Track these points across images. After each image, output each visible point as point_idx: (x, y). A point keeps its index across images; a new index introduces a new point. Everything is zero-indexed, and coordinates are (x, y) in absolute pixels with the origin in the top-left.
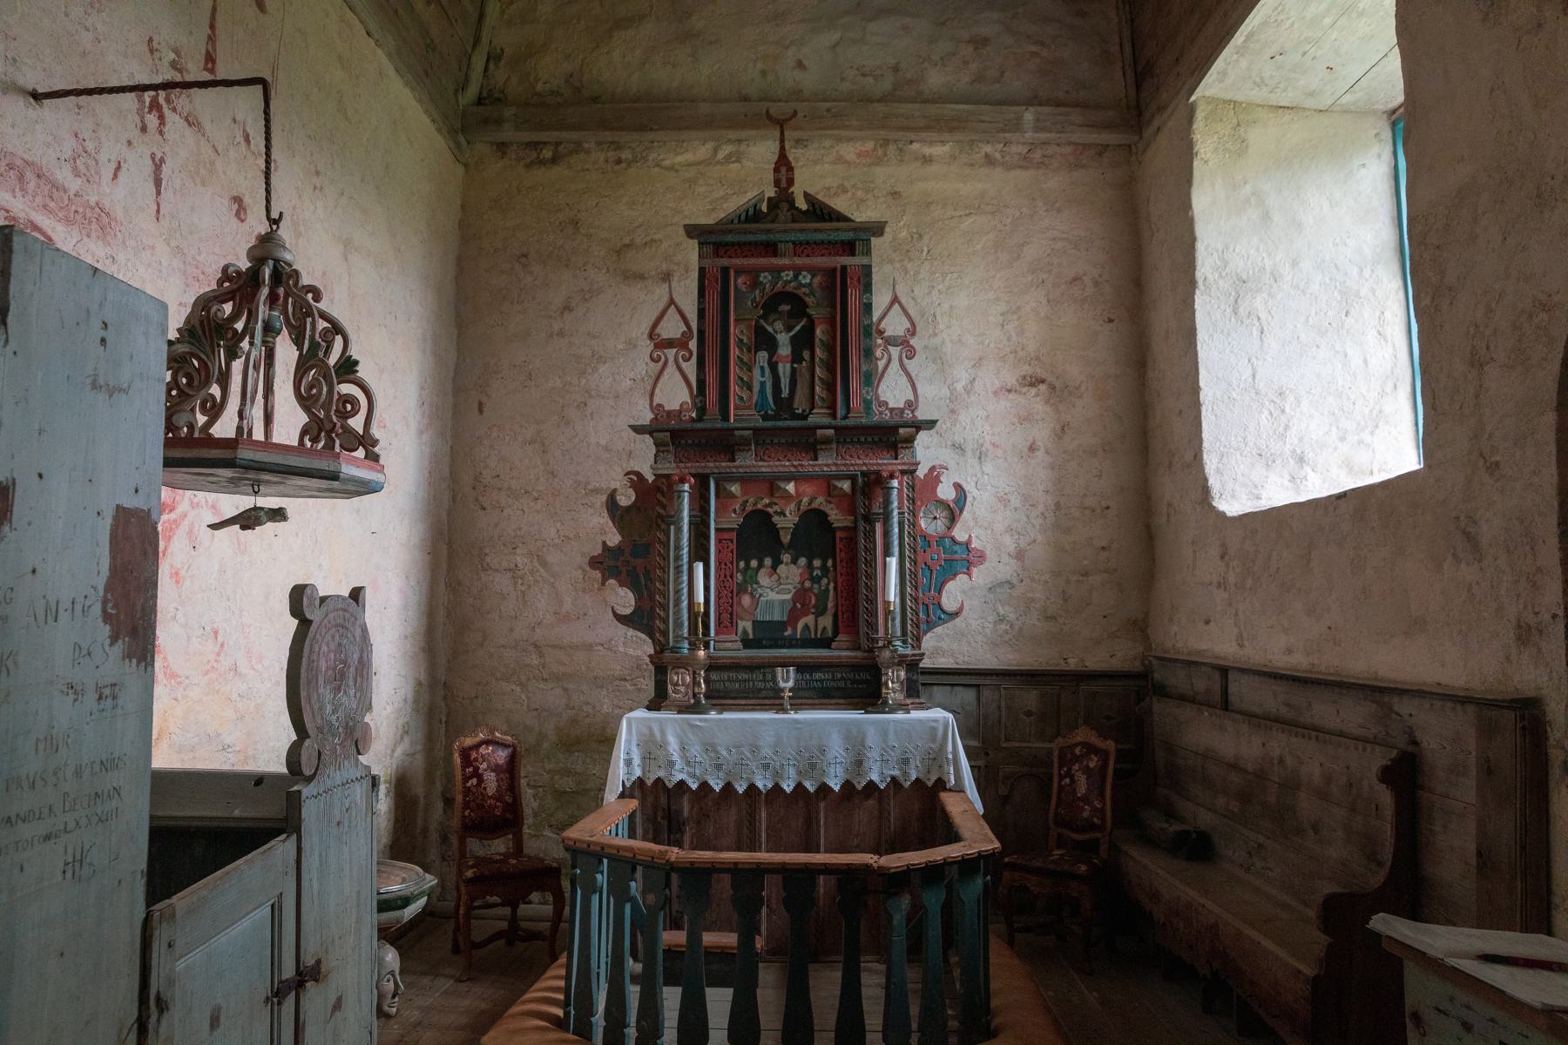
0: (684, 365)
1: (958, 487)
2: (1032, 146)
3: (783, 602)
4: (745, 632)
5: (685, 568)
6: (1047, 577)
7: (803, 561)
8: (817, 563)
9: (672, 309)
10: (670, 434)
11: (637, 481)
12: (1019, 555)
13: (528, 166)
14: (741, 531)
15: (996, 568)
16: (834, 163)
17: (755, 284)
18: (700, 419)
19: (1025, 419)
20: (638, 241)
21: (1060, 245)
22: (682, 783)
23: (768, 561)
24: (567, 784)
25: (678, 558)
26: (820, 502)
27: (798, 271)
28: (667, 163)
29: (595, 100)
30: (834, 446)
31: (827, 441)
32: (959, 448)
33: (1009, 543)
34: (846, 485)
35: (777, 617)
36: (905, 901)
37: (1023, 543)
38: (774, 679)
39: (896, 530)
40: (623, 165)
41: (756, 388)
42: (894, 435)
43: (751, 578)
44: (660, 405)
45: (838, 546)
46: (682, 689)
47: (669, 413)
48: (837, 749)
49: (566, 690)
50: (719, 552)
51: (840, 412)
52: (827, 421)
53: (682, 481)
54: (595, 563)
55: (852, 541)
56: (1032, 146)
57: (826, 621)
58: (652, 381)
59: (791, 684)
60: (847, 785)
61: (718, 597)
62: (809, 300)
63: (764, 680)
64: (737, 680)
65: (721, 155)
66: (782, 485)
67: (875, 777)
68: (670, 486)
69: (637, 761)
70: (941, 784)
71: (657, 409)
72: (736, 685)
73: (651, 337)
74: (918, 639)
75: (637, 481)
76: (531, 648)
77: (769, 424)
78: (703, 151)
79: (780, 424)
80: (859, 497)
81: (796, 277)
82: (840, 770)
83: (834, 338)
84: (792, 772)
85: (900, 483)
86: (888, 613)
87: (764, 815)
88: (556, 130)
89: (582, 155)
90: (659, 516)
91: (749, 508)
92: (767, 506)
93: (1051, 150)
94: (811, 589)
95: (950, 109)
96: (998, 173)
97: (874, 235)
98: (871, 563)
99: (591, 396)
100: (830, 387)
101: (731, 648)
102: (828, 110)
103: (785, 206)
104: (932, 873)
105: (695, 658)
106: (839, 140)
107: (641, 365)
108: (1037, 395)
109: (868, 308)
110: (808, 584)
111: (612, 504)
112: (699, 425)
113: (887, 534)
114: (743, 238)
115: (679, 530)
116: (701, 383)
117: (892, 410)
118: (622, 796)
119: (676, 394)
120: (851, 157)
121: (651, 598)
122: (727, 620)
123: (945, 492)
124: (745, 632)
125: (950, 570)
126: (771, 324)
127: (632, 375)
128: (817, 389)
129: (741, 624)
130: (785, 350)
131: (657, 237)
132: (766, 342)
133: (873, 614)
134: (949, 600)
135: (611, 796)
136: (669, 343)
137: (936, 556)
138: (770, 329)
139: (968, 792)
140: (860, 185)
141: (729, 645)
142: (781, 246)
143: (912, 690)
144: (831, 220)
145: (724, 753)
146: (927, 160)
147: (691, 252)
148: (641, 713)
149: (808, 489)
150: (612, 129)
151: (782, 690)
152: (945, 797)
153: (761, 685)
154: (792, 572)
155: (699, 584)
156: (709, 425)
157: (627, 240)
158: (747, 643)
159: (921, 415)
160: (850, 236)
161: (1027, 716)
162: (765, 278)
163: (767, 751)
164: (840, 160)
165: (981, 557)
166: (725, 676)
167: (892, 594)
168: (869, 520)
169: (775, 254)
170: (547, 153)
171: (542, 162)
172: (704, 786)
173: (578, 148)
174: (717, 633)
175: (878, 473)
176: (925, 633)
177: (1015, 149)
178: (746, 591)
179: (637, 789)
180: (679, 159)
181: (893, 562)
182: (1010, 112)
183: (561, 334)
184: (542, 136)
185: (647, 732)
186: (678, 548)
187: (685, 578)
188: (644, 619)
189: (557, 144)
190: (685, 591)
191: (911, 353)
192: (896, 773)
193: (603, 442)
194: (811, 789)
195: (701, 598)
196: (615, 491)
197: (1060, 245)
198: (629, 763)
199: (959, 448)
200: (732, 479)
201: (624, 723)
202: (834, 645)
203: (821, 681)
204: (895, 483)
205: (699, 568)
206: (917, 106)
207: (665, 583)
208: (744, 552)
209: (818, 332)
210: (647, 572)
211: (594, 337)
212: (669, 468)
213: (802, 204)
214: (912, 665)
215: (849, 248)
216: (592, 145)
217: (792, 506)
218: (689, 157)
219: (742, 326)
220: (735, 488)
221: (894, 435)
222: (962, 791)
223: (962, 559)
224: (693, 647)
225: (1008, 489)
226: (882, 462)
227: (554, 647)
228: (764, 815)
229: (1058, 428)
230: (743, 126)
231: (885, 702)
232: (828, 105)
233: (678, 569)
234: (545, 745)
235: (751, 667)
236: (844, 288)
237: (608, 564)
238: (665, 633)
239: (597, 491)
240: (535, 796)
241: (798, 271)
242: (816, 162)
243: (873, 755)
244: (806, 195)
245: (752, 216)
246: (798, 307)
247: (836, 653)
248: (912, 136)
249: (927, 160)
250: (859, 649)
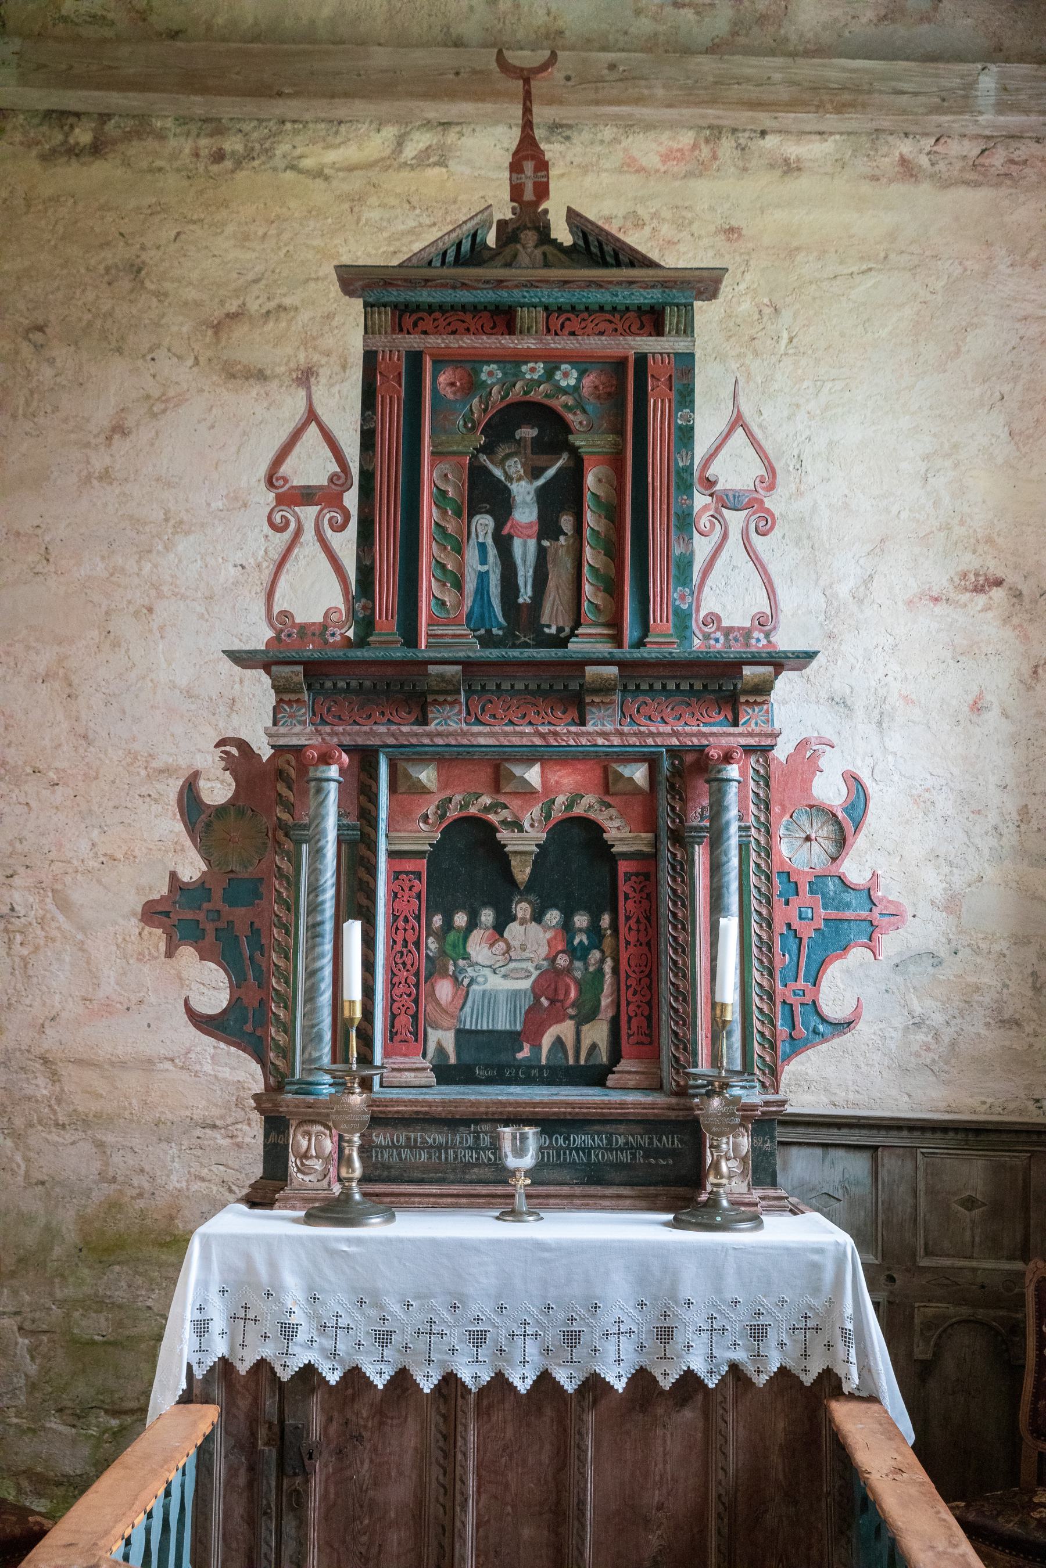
0: (336, 540)
1: (853, 780)
2: (989, 142)
3: (515, 994)
4: (441, 1050)
5: (328, 927)
6: (1002, 946)
7: (553, 916)
8: (581, 920)
9: (313, 427)
10: (305, 670)
11: (238, 756)
12: (952, 904)
13: (47, 158)
14: (436, 855)
15: (919, 930)
16: (620, 171)
17: (472, 386)
18: (361, 641)
19: (965, 653)
20: (253, 306)
21: (1033, 330)
22: (309, 1369)
23: (487, 916)
24: (95, 1326)
25: (314, 908)
26: (588, 805)
27: (553, 362)
28: (308, 163)
29: (174, 35)
30: (617, 697)
31: (604, 689)
32: (841, 704)
33: (933, 883)
34: (639, 774)
35: (502, 1024)
37: (959, 881)
38: (496, 1147)
39: (735, 862)
40: (228, 164)
41: (470, 585)
42: (729, 681)
44: (285, 614)
45: (623, 891)
46: (318, 1165)
47: (303, 628)
48: (619, 1300)
49: (100, 1145)
50: (394, 896)
51: (630, 632)
52: (604, 649)
53: (326, 759)
54: (152, 913)
56: (989, 142)
57: (597, 1033)
58: (272, 568)
59: (528, 1161)
60: (642, 1378)
61: (391, 984)
62: (574, 419)
63: (476, 1148)
64: (425, 1146)
65: (410, 151)
66: (517, 770)
67: (698, 1364)
68: (303, 769)
69: (218, 1323)
70: (830, 1383)
72: (424, 1157)
73: (270, 482)
74: (774, 1072)
75: (238, 756)
76: (38, 1065)
77: (494, 654)
78: (376, 143)
79: (515, 653)
80: (663, 796)
81: (549, 374)
82: (627, 1346)
83: (620, 491)
84: (532, 1349)
85: (743, 772)
86: (719, 1027)
87: (472, 1438)
88: (98, 87)
89: (151, 144)
90: (281, 825)
91: (453, 814)
92: (487, 809)
93: (1025, 150)
94: (568, 970)
95: (837, 70)
96: (924, 193)
97: (701, 295)
98: (685, 924)
99: (160, 596)
100: (612, 587)
101: (408, 1079)
102: (612, 67)
103: (530, 237)
105: (347, 1110)
106: (630, 126)
107: (260, 543)
108: (987, 609)
109: (686, 435)
110: (562, 961)
111: (190, 801)
112: (360, 654)
113: (716, 868)
114: (450, 296)
115: (317, 853)
116: (365, 573)
117: (728, 631)
118: (186, 1398)
119: (316, 594)
120: (652, 160)
121: (262, 983)
122: (407, 1029)
123: (829, 790)
124: (441, 1050)
125: (835, 939)
126: (501, 463)
127: (239, 557)
128: (587, 589)
129: (434, 1036)
130: (525, 514)
131: (287, 301)
132: (488, 496)
133: (688, 1021)
135: (164, 1396)
136: (306, 496)
137: (805, 913)
138: (498, 473)
139: (887, 1401)
140: (666, 214)
141: (409, 1077)
142: (522, 313)
143: (762, 1171)
144: (618, 264)
145: (396, 1308)
146: (790, 168)
147: (348, 329)
148: (235, 1221)
149: (567, 779)
150: (205, 91)
151: (513, 1173)
152: (842, 1412)
153: (470, 1156)
154: (533, 938)
155: (347, 964)
156: (379, 654)
157: (232, 307)
158: (446, 1074)
159: (785, 641)
160: (654, 296)
162: (490, 374)
163: (481, 1306)
164: (631, 166)
165: (896, 915)
166: (401, 1136)
167: (729, 993)
168: (681, 838)
169: (510, 329)
170: (83, 136)
171: (73, 152)
172: (354, 1376)
173: (141, 127)
174: (386, 1055)
175: (701, 751)
176: (788, 1059)
177: (955, 148)
178: (444, 974)
179: (217, 1384)
180: (331, 156)
181: (730, 926)
182: (951, 75)
183: (106, 476)
184: (71, 99)
185: (241, 1264)
186: (315, 889)
187: (328, 947)
188: (242, 1025)
189: (104, 117)
190: (328, 972)
192: (740, 1355)
193: (183, 682)
194: (570, 1387)
195: (354, 991)
196: (196, 775)
197: (1033, 330)
198: (202, 1328)
199: (841, 704)
200: (422, 756)
201: (195, 1247)
202: (611, 1080)
203: (587, 1150)
204: (733, 771)
205: (354, 930)
206: (779, 61)
207: (289, 954)
209: (590, 480)
210: (255, 932)
211: (169, 485)
212: (301, 733)
213: (562, 234)
215: (653, 319)
216: (169, 123)
217: (536, 811)
219: (445, 467)
220: (427, 776)
221: (729, 681)
222: (873, 1399)
223: (851, 918)
225: (930, 782)
226: (712, 732)
227: (80, 1062)
228: (472, 1438)
229: (1026, 670)
230: (451, 95)
231: (713, 1203)
232: (611, 56)
233: (314, 928)
234: (57, 1251)
235: (452, 1122)
236: (641, 399)
237: (180, 917)
238: (286, 1052)
239: (167, 771)
240: (33, 1351)
241: (553, 362)
242: (585, 169)
243: (691, 1322)
244: (572, 215)
245: (468, 253)
246: (553, 431)
247: (616, 1097)
248: (765, 119)
249: (790, 168)
250: (658, 1087)
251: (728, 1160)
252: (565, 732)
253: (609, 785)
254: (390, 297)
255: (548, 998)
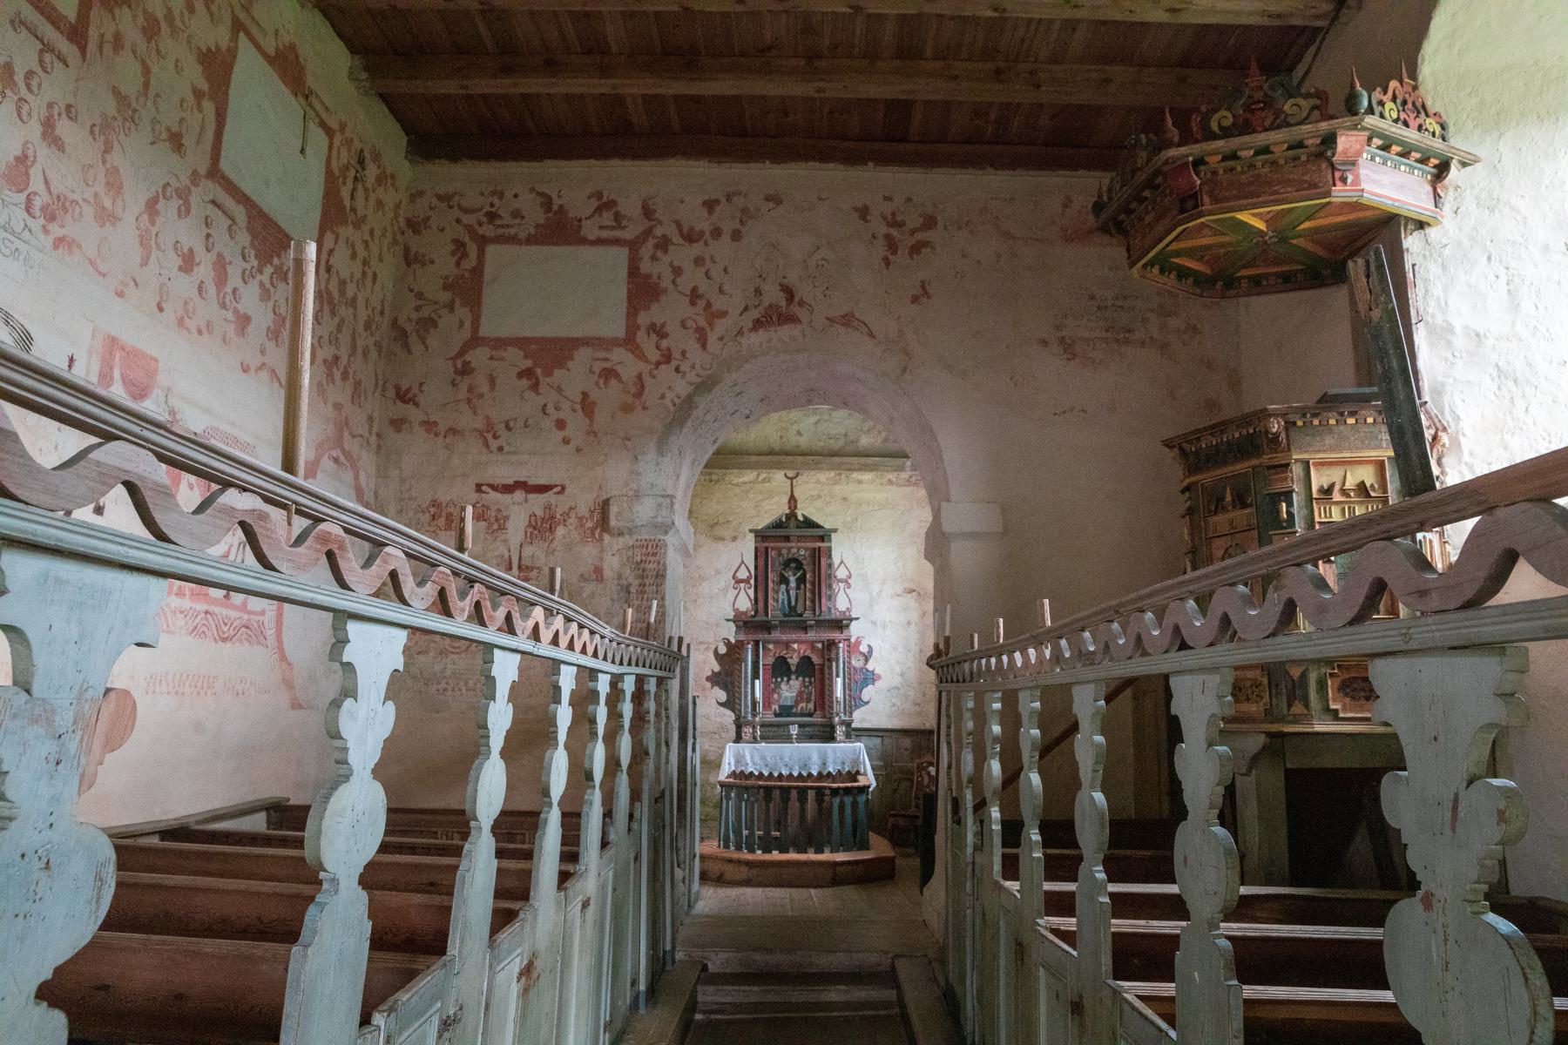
10: (744, 623)
11: (728, 643)
12: (902, 675)
17: (780, 554)
19: (906, 609)
33: (898, 669)
34: (820, 645)
36: (837, 800)
42: (840, 624)
43: (778, 686)
45: (816, 671)
55: (822, 670)
57: (811, 706)
60: (820, 773)
70: (858, 773)
71: (736, 610)
72: (774, 733)
75: (728, 643)
100: (813, 601)
101: (770, 718)
104: (847, 791)
109: (830, 566)
111: (716, 652)
119: (745, 604)
123: (863, 648)
130: (793, 584)
134: (390, 704)
136: (742, 581)
143: (848, 736)
149: (803, 647)
154: (796, 684)
158: (776, 715)
161: (909, 750)
162: (784, 552)
165: (879, 677)
168: (830, 660)
172: (761, 774)
181: (839, 681)
188: (730, 704)
191: (849, 586)
208: (775, 675)
214: (848, 724)
215: (822, 539)
218: (745, 479)
221: (840, 624)
223: (870, 678)
224: (754, 716)
226: (836, 635)
235: (779, 725)
237: (715, 679)
245: (778, 525)
246: (799, 565)
249: (860, 482)
251: (840, 731)
252: (803, 636)
253: (813, 648)
254: (761, 536)
255: (800, 697)
